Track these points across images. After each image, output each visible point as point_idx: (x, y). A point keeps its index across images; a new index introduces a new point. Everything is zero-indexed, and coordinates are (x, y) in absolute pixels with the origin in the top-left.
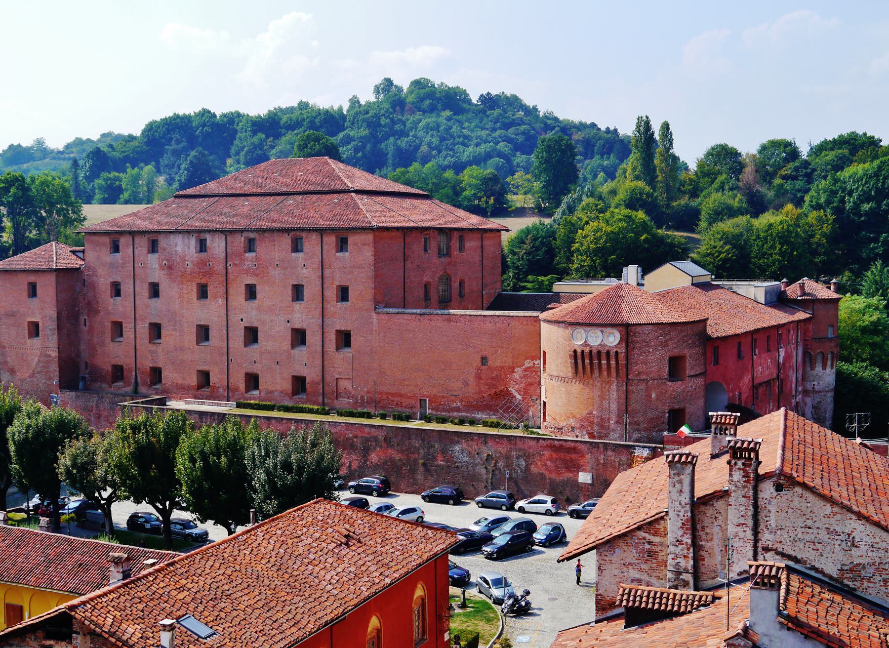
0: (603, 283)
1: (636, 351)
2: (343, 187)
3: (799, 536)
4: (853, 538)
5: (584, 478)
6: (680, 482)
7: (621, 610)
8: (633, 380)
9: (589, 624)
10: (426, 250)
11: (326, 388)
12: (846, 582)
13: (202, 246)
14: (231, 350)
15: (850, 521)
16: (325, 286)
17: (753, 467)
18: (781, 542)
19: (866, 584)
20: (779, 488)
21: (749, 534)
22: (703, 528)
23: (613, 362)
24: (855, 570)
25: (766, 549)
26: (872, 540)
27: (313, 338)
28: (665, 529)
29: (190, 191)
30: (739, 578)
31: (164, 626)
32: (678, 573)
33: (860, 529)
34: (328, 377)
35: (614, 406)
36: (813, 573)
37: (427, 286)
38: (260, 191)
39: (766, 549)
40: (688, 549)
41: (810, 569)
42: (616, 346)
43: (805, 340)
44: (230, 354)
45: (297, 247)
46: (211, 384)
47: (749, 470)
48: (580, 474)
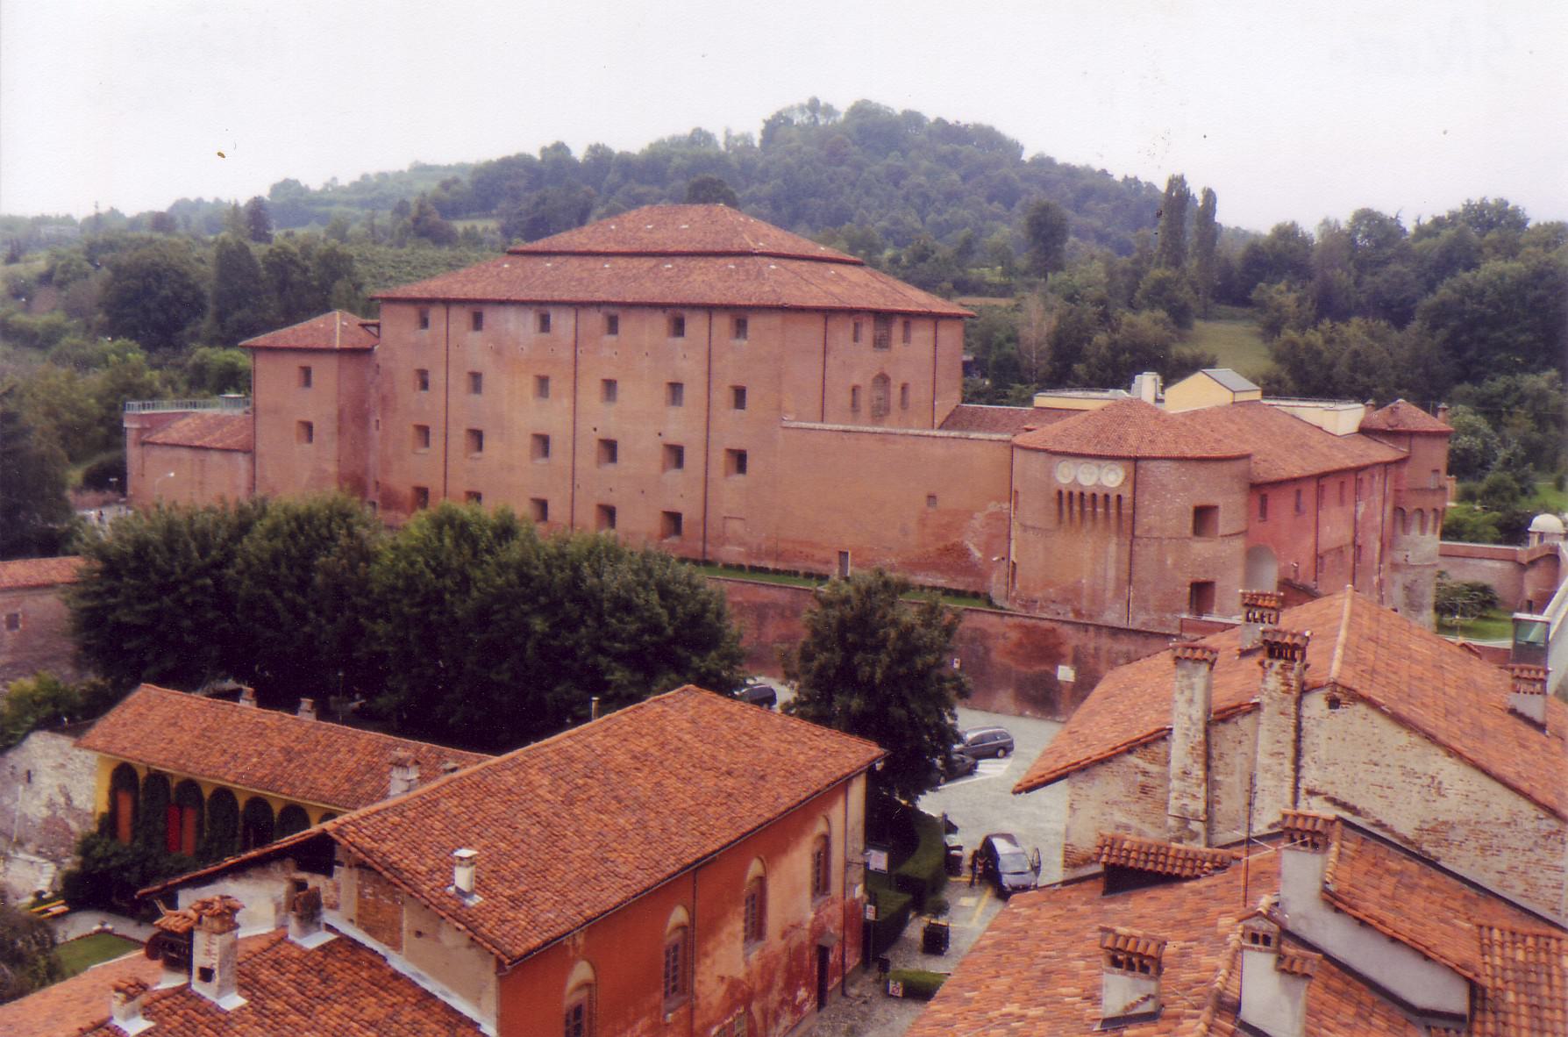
0: (1105, 395)
1: (1147, 496)
2: (745, 248)
3: (1361, 775)
4: (1440, 783)
5: (1065, 673)
6: (1191, 687)
7: (1098, 868)
8: (1141, 538)
9: (1054, 885)
10: (856, 339)
11: (709, 531)
12: (1425, 847)
13: (545, 324)
14: (578, 473)
15: (1436, 758)
16: (712, 386)
17: (1296, 671)
18: (1332, 783)
19: (1455, 852)
20: (1334, 703)
21: (1288, 767)
22: (1221, 756)
23: (1113, 511)
24: (1440, 830)
25: (1311, 793)
26: (1467, 788)
27: (693, 457)
28: (1168, 754)
29: (540, 245)
30: (1270, 832)
31: (461, 859)
32: (1184, 820)
33: (1449, 770)
34: (711, 516)
35: (1112, 573)
36: (1377, 831)
37: (855, 390)
38: (625, 249)
39: (1311, 793)
40: (1199, 786)
41: (1374, 825)
42: (1118, 488)
43: (1397, 491)
44: (577, 477)
45: (678, 328)
46: (549, 518)
47: (1291, 675)
48: (1060, 667)
